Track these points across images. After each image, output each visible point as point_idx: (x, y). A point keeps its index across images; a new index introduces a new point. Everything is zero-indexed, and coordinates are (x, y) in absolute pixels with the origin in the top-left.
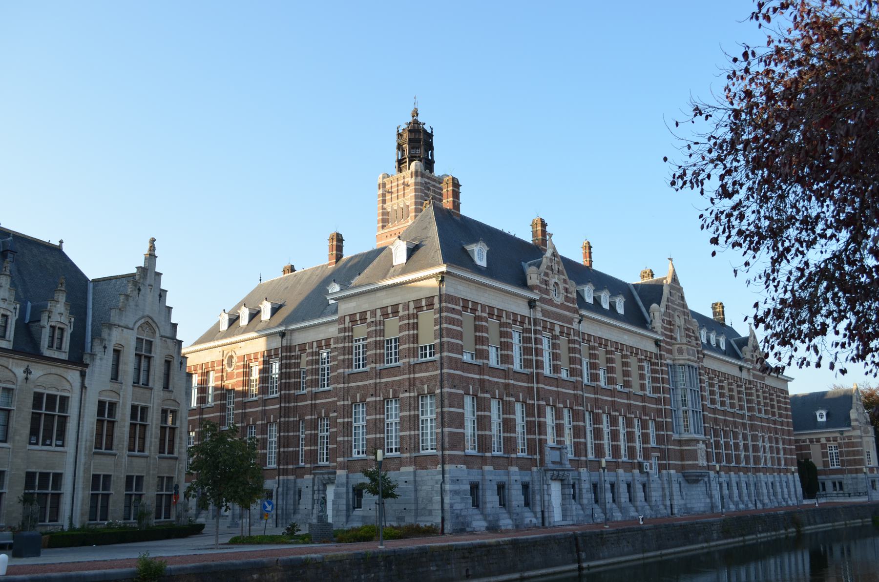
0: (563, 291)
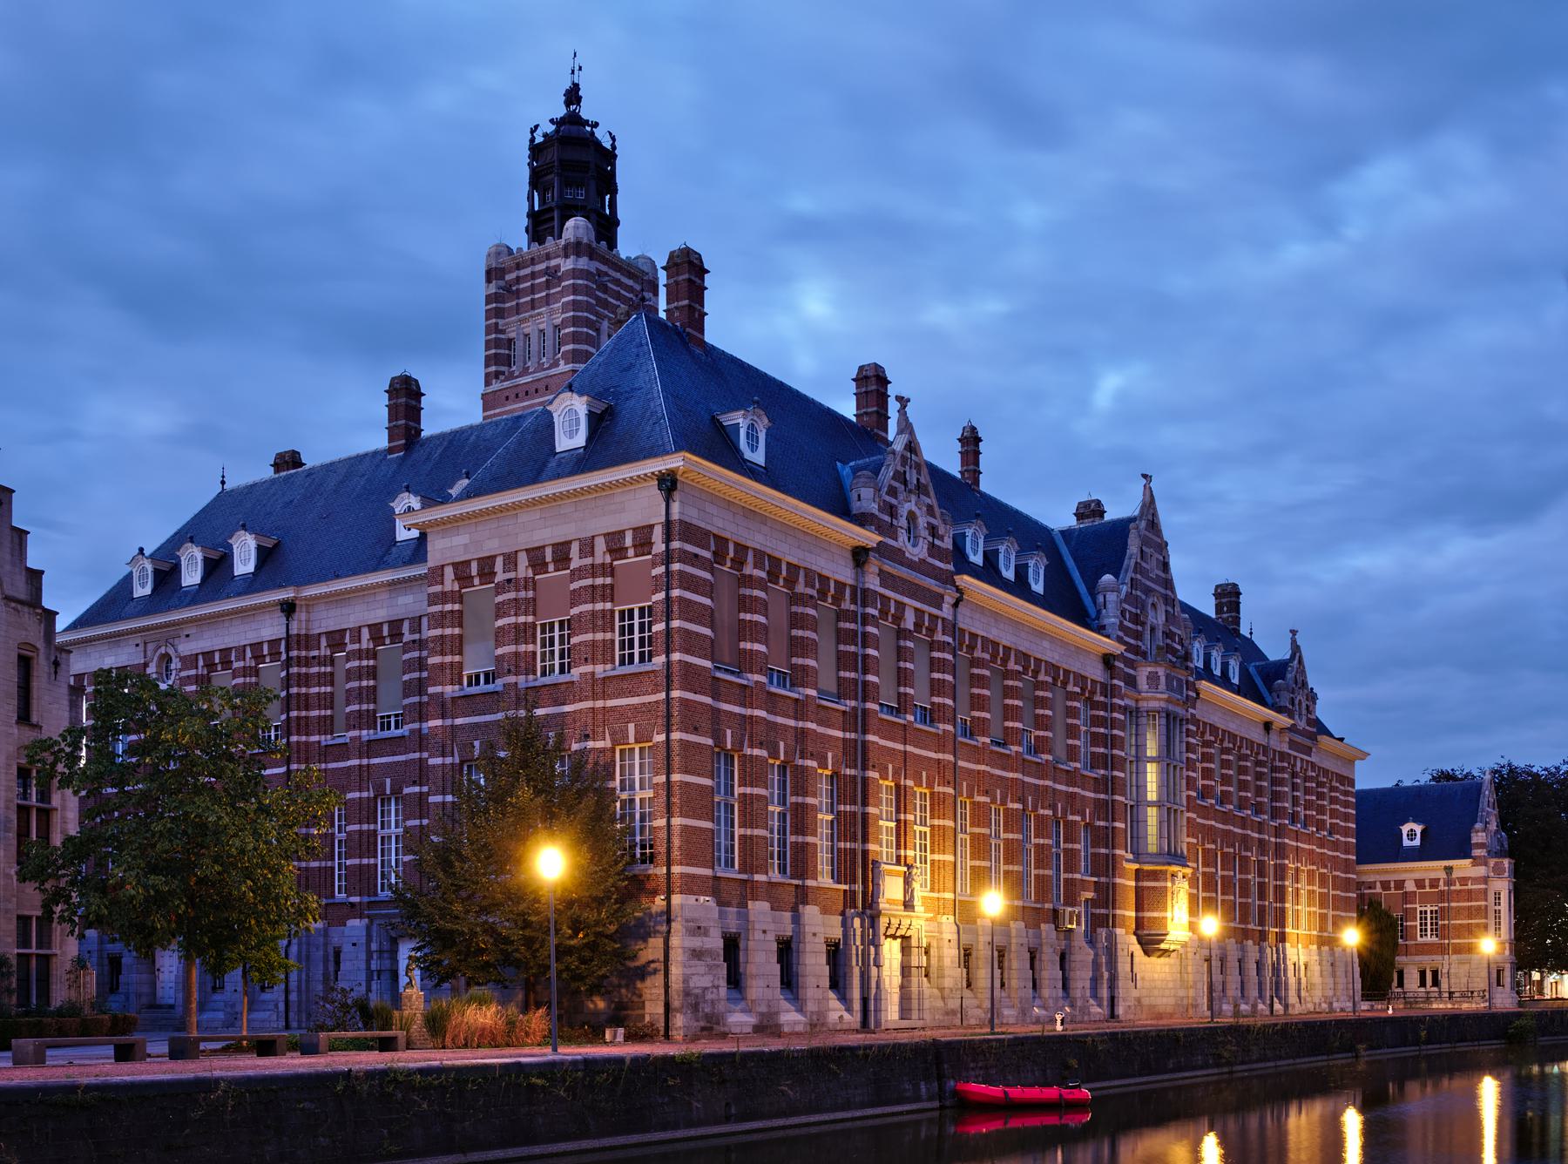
0: (925, 533)
